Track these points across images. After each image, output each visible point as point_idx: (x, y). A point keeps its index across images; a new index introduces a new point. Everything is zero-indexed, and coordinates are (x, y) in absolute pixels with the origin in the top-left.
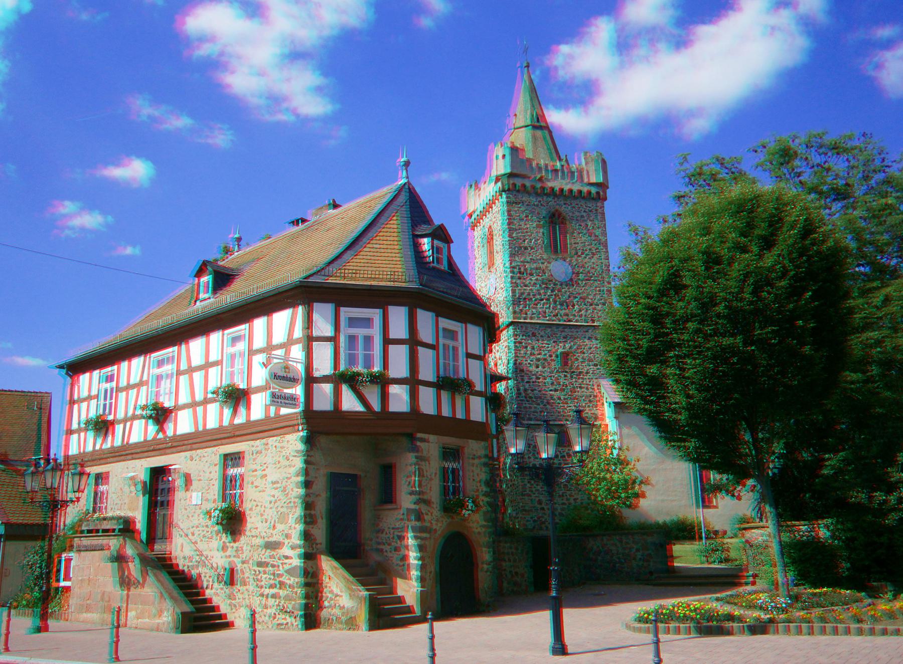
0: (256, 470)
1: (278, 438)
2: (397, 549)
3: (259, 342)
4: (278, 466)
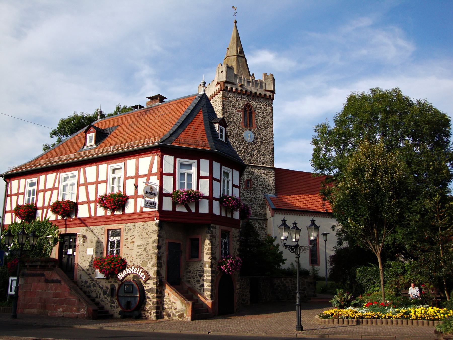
0: (127, 239)
1: (142, 223)
2: (198, 281)
3: (131, 172)
4: (141, 237)
